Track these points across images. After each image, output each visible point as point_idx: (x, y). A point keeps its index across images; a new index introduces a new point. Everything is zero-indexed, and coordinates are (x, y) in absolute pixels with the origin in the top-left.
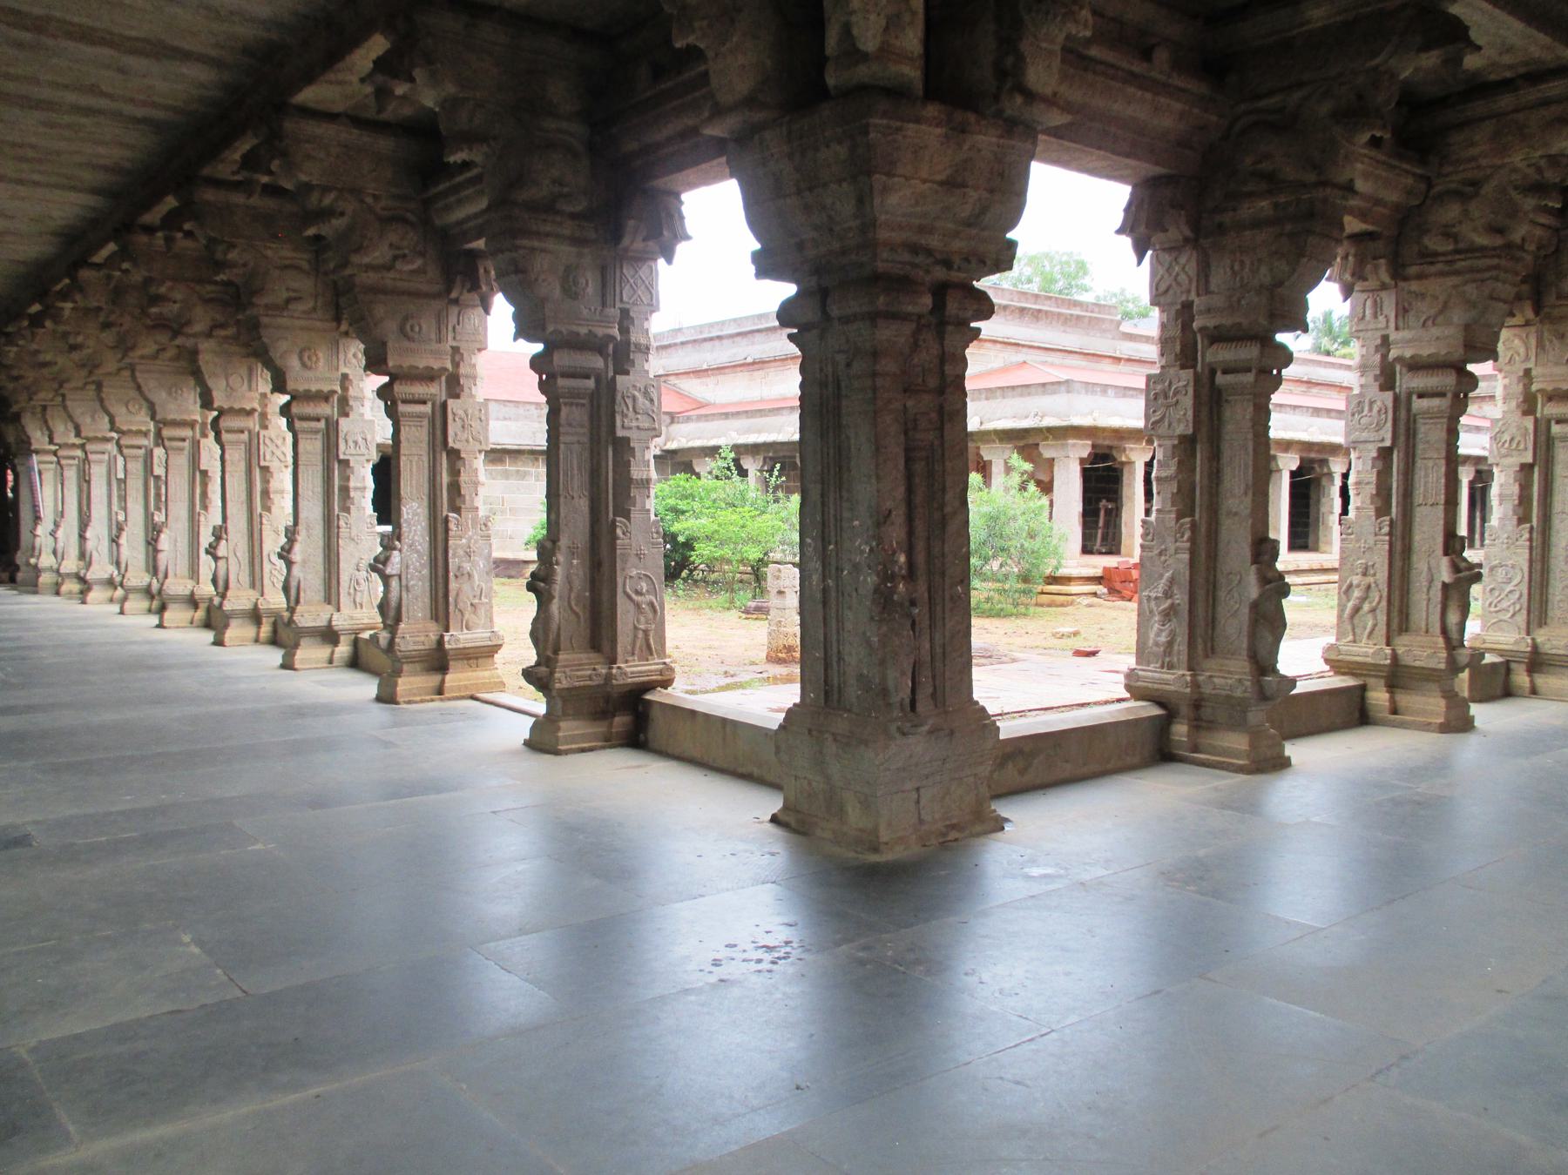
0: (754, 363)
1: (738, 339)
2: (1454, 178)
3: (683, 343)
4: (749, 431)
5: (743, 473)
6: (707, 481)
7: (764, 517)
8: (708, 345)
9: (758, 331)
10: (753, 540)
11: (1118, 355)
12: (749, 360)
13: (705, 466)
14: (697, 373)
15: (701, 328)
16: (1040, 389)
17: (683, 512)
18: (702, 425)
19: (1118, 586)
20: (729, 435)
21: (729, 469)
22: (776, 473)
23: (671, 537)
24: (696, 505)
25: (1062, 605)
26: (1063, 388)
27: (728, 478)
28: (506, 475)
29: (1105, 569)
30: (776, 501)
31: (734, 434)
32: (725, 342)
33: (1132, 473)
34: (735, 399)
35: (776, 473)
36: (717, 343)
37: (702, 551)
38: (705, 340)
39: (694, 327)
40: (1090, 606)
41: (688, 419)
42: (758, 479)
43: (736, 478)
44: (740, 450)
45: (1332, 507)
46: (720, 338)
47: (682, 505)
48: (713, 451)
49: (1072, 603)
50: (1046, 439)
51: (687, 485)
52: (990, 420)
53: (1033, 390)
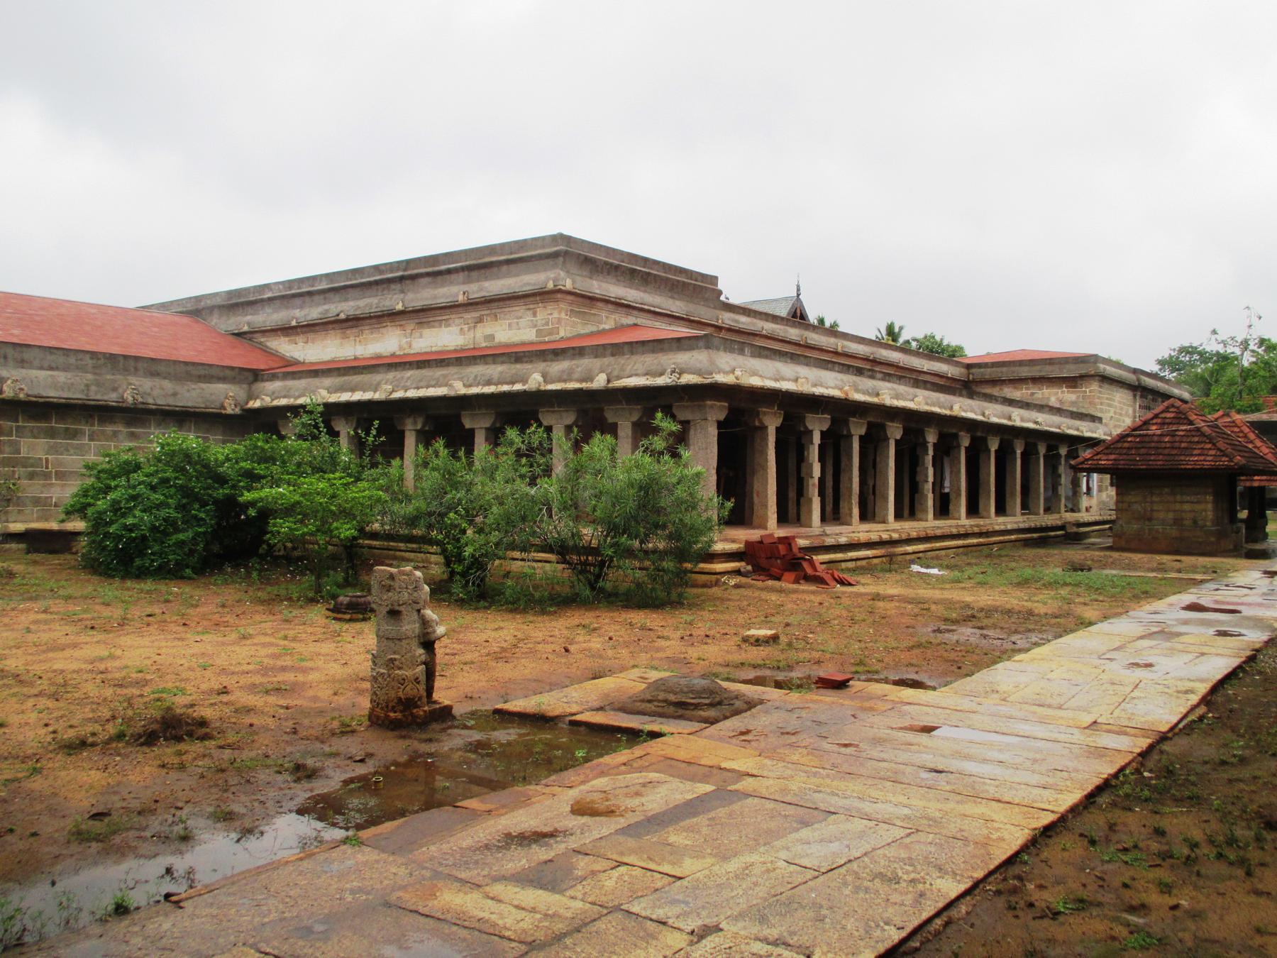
0: (347, 320)
1: (331, 295)
2: (77, 653)
3: (270, 299)
4: (342, 389)
5: (334, 434)
6: (291, 443)
7: (360, 484)
8: (298, 301)
9: (352, 286)
10: (345, 513)
11: (720, 323)
12: (342, 316)
13: (293, 427)
14: (286, 330)
15: (290, 283)
16: (674, 345)
17: (261, 477)
18: (290, 383)
19: (763, 563)
20: (324, 393)
21: (316, 427)
22: (374, 432)
23: (230, 506)
24: (276, 469)
25: (704, 586)
26: (701, 343)
27: (315, 438)
28: (52, 434)
29: (748, 543)
30: (374, 465)
31: (324, 393)
32: (316, 298)
33: (765, 439)
34: (327, 357)
35: (374, 432)
36: (307, 299)
37: (282, 526)
38: (294, 296)
39: (282, 283)
40: (737, 586)
41: (274, 377)
42: (351, 438)
43: (324, 438)
44: (332, 410)
45: (927, 476)
46: (310, 294)
47: (260, 469)
48: (296, 410)
49: (717, 583)
50: (681, 399)
51: (533, 491)
52: (619, 378)
53: (666, 346)
